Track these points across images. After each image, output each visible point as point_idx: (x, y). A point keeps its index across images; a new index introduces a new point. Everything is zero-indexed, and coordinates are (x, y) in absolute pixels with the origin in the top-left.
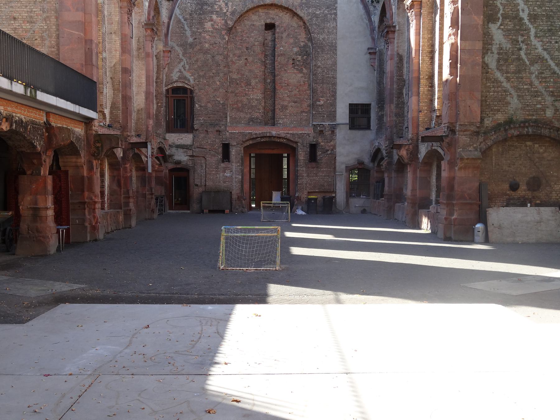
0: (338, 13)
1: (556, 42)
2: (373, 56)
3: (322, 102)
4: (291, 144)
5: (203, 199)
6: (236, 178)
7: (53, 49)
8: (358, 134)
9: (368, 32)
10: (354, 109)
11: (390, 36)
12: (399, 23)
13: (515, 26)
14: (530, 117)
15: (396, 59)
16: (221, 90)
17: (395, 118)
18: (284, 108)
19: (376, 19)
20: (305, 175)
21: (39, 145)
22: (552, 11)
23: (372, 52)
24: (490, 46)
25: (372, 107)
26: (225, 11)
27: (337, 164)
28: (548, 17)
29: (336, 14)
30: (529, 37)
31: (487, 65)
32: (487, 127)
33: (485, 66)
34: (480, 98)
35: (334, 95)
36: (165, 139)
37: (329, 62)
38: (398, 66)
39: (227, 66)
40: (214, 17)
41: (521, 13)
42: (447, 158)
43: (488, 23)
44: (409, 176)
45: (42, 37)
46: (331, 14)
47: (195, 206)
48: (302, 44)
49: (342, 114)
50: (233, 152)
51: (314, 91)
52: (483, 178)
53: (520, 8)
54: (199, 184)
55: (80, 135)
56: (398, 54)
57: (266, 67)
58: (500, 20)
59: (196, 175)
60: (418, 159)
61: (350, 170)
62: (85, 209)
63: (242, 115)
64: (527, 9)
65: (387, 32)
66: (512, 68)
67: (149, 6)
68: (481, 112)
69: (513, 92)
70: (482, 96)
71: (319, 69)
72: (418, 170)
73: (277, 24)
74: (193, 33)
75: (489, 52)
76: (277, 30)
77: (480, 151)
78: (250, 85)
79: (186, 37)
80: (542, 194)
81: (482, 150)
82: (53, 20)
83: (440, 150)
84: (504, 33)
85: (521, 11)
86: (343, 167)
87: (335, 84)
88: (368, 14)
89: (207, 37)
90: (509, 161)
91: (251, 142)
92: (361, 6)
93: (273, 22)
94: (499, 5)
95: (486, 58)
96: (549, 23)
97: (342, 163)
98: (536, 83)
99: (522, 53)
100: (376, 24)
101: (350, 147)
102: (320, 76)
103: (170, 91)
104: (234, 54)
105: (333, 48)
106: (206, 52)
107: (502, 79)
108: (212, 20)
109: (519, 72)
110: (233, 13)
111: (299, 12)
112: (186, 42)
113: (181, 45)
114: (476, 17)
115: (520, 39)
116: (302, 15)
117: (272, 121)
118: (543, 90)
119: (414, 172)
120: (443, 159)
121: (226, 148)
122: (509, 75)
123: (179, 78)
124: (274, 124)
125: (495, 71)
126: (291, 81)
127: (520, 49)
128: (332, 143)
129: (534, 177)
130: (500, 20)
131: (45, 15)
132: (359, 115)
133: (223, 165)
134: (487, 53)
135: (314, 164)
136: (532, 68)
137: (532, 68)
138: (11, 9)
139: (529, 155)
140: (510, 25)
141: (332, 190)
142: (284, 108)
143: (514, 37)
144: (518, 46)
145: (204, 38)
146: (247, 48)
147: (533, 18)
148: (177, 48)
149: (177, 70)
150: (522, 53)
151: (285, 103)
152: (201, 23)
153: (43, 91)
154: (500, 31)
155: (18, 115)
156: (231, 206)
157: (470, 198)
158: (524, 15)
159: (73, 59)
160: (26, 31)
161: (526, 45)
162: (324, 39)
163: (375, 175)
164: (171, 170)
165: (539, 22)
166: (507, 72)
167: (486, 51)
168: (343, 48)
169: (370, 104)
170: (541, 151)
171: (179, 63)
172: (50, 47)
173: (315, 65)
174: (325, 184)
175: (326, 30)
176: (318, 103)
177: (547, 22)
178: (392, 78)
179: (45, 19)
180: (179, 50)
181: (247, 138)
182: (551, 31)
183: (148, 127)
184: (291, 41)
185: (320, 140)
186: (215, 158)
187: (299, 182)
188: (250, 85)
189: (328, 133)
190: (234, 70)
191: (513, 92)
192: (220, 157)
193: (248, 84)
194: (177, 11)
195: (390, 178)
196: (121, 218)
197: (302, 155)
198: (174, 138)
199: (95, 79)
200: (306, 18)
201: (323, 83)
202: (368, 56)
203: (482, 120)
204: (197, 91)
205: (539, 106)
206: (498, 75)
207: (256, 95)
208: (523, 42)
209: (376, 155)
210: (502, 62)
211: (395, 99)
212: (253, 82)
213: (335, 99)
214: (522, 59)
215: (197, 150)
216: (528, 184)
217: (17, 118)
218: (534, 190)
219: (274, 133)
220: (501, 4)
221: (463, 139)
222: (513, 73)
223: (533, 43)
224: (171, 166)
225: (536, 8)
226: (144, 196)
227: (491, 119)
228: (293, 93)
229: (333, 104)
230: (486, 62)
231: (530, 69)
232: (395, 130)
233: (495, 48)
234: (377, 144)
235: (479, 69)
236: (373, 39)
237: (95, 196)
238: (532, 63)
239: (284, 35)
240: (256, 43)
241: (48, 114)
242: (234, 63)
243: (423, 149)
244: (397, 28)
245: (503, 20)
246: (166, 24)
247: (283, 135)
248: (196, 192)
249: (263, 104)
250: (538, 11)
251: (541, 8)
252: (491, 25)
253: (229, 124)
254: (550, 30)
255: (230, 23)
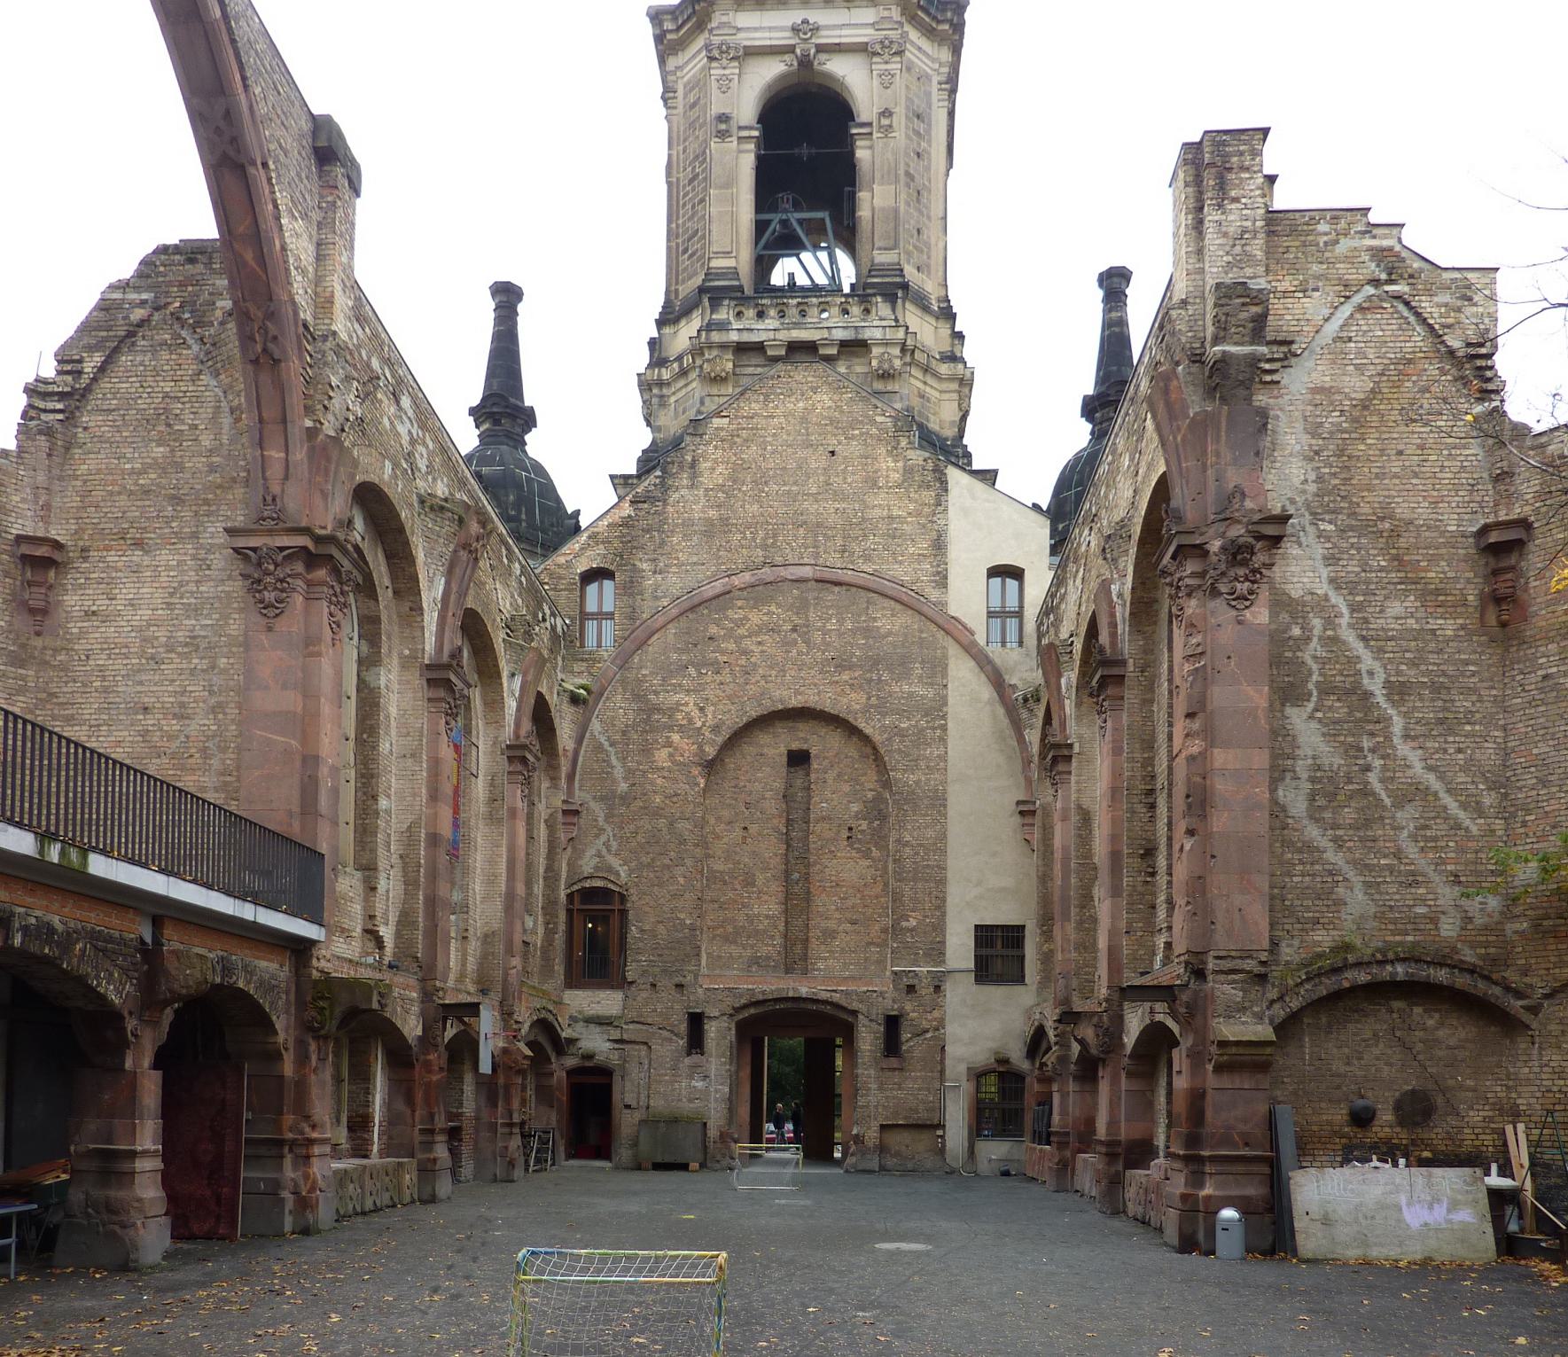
0: (950, 725)
1: (1460, 751)
2: (1028, 820)
3: (913, 922)
4: (845, 1016)
5: (641, 1138)
6: (716, 1091)
7: (228, 779)
8: (996, 993)
9: (1018, 766)
10: (984, 935)
11: (1061, 767)
12: (1080, 737)
13: (1350, 713)
14: (1398, 938)
15: (1074, 818)
16: (687, 895)
17: (1074, 955)
18: (830, 934)
19: (1033, 737)
20: (874, 1086)
21: (115, 990)
22: (1444, 674)
23: (1026, 812)
24: (1289, 762)
25: (1027, 933)
26: (699, 724)
27: (947, 1062)
28: (1436, 688)
29: (944, 728)
30: (1388, 738)
31: (1284, 809)
32: (1287, 963)
33: (1278, 812)
34: (1266, 889)
35: (940, 905)
36: (559, 1003)
37: (930, 833)
38: (1080, 836)
39: (703, 843)
40: (676, 737)
41: (1366, 681)
42: (1186, 1043)
43: (1283, 705)
44: (1104, 1087)
45: (204, 750)
46: (934, 729)
47: (623, 1153)
48: (870, 795)
49: (960, 950)
50: (712, 1030)
51: (897, 898)
52: (1279, 1093)
53: (1363, 667)
54: (634, 1104)
55: (273, 977)
56: (1079, 807)
57: (789, 846)
58: (1314, 699)
59: (628, 1084)
60: (1123, 1045)
61: (978, 1075)
62: (282, 1157)
63: (735, 950)
64: (1381, 670)
65: (1055, 759)
66: (1349, 814)
67: (519, 709)
68: (1271, 925)
69: (1351, 875)
70: (1272, 887)
71: (907, 850)
72: (1123, 1076)
73: (813, 751)
74: (630, 772)
75: (1289, 775)
76: (815, 765)
77: (1271, 1022)
78: (753, 885)
79: (614, 781)
80: (1437, 1134)
81: (1277, 1021)
82: (232, 711)
83: (1171, 1023)
84: (1325, 730)
85: (1365, 675)
86: (963, 1068)
87: (942, 882)
88: (1018, 726)
89: (659, 781)
90: (1346, 1050)
91: (752, 1011)
92: (1001, 711)
93: (805, 747)
94: (1310, 661)
95: (1281, 792)
96: (1440, 703)
97: (961, 1060)
98: (1412, 851)
99: (1373, 778)
100: (1035, 749)
101: (980, 1026)
102: (908, 864)
103: (577, 898)
104: (719, 819)
105: (939, 802)
106: (657, 813)
107: (1324, 843)
108: (669, 744)
109: (1367, 823)
110: (716, 729)
111: (862, 725)
112: (613, 792)
113: (602, 799)
114: (1250, 691)
115: (1366, 743)
116: (868, 731)
117: (795, 958)
118: (1430, 870)
119: (1115, 1081)
120: (1177, 1044)
121: (696, 1022)
122: (1340, 832)
123: (596, 868)
124: (805, 972)
125: (1305, 822)
126: (844, 875)
127: (1367, 768)
128: (936, 1014)
129: (1413, 1092)
130: (1314, 699)
131: (213, 701)
132: (998, 952)
133: (687, 1061)
134: (1283, 779)
135: (893, 1062)
136: (1399, 815)
137: (1399, 815)
138: (139, 688)
139: (1398, 1034)
140: (1341, 711)
141: (936, 1122)
142: (830, 934)
143: (1350, 739)
144: (1361, 762)
145: (652, 783)
146: (747, 805)
147: (1398, 691)
148: (592, 804)
149: (593, 851)
150: (1373, 778)
151: (832, 924)
152: (647, 751)
153: (105, 853)
154: (1314, 725)
155: (38, 913)
156: (705, 1153)
157: (1247, 1144)
158: (1376, 686)
159: (274, 805)
160: (171, 738)
161: (1383, 757)
162: (917, 782)
163: (1037, 1087)
164: (571, 1072)
165: (1413, 701)
166: (1335, 827)
167: (1278, 773)
168: (959, 801)
169: (1023, 927)
170: (1430, 1023)
171: (597, 836)
172: (223, 774)
173: (898, 841)
174: (921, 1107)
175: (922, 764)
176: (904, 924)
177: (1433, 700)
178: (1066, 860)
179: (213, 710)
180: (598, 809)
181: (743, 1001)
182: (1446, 724)
183: (506, 975)
184: (846, 788)
185: (908, 1007)
186: (669, 1047)
187: (861, 1101)
188: (753, 885)
189: (925, 991)
190: (719, 853)
191: (1351, 875)
192: (682, 1042)
193: (749, 882)
194: (596, 726)
195: (1065, 1095)
196: (408, 1178)
197: (868, 1039)
198: (585, 1001)
199: (323, 848)
200: (877, 738)
201: (915, 880)
202: (1018, 819)
203: (1274, 944)
204: (634, 898)
205: (1421, 910)
206: (1313, 832)
207: (768, 907)
208: (1373, 751)
209: (1036, 1042)
210: (1321, 802)
211: (1073, 911)
212: (760, 879)
213: (944, 914)
214: (1374, 794)
215: (631, 1026)
216: (1398, 1107)
217: (33, 921)
218: (1416, 1124)
219: (804, 991)
220: (1315, 657)
221: (1225, 991)
222: (1351, 827)
223: (1399, 753)
224: (571, 1062)
225: (1404, 667)
226: (493, 1128)
227: (1296, 942)
228: (849, 903)
229: (939, 927)
230: (1281, 800)
231: (1393, 818)
232: (1074, 983)
233: (1302, 767)
234: (1038, 1016)
235: (1262, 817)
236: (1029, 781)
237: (314, 1127)
238: (1402, 800)
239: (831, 776)
240: (768, 795)
241: (157, 922)
242: (718, 837)
243: (1134, 1023)
244: (1076, 749)
245: (1320, 699)
246: (570, 754)
247: (824, 996)
248: (626, 1123)
249: (781, 927)
250: (1410, 674)
251: (1417, 665)
252: (1290, 711)
253: (704, 971)
254: (1441, 722)
255: (711, 751)
